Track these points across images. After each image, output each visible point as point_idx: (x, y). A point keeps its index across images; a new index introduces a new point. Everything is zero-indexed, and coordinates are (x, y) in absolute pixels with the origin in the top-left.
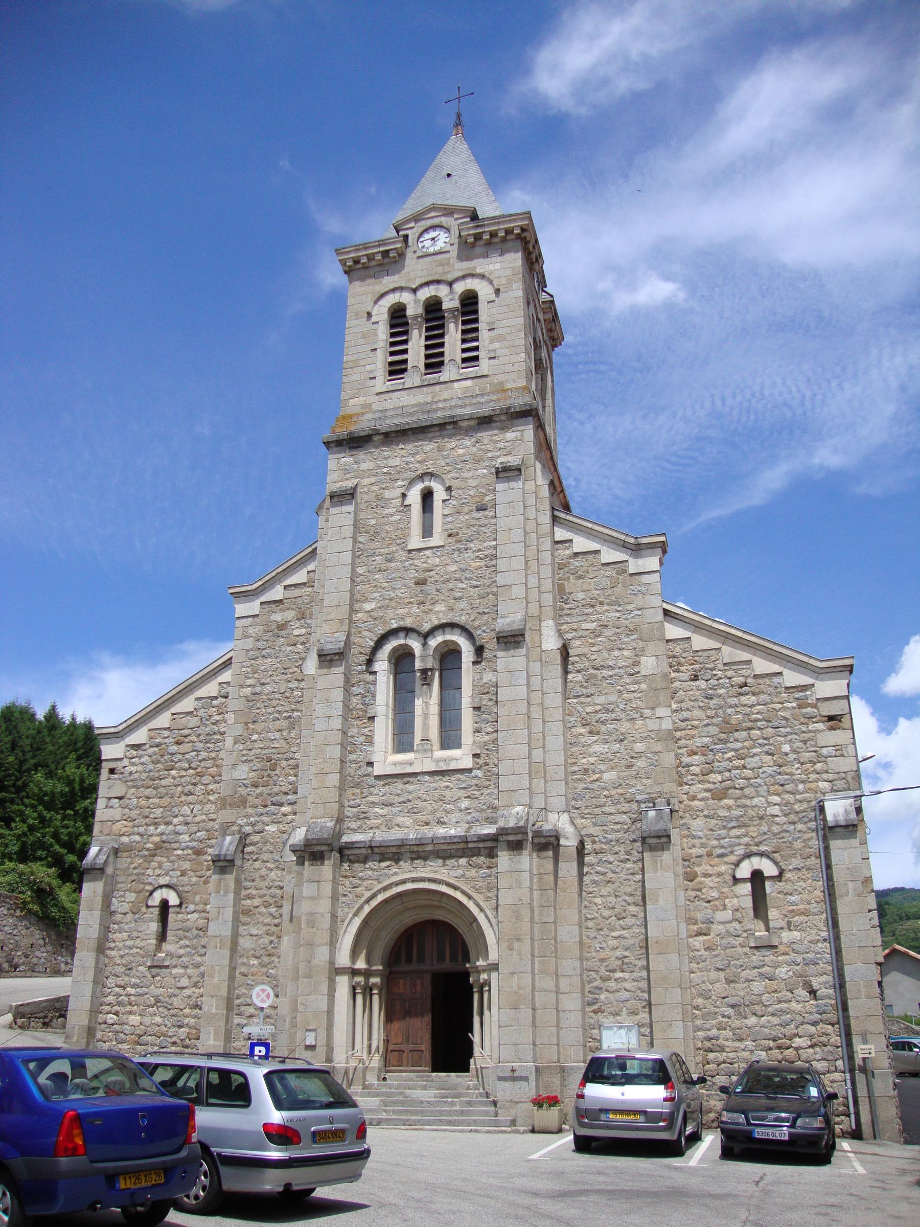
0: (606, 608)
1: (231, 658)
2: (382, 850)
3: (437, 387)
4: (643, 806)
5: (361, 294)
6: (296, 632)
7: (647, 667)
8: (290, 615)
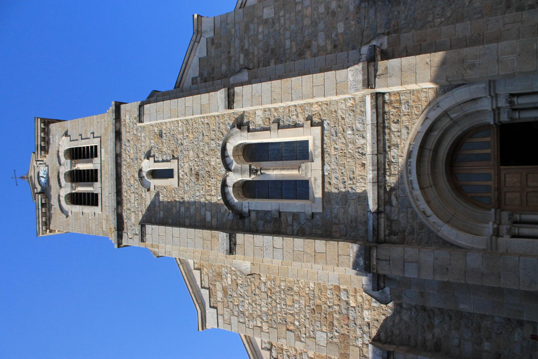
0: (232, 49)
1: (245, 336)
2: (382, 203)
3: (102, 171)
6: (230, 283)
7: (269, 13)
8: (219, 286)
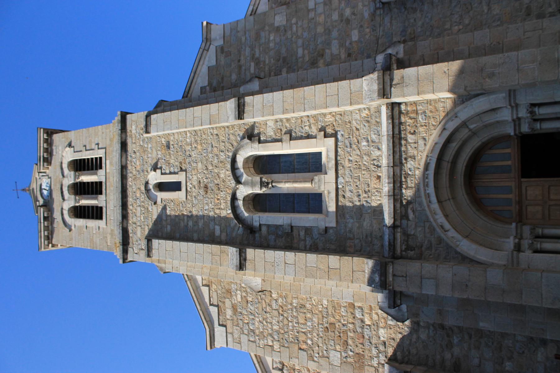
1: (256, 355)
3: (107, 184)
4: (378, 5)
5: (61, 236)
6: (239, 300)
7: (281, 21)
8: (228, 303)
